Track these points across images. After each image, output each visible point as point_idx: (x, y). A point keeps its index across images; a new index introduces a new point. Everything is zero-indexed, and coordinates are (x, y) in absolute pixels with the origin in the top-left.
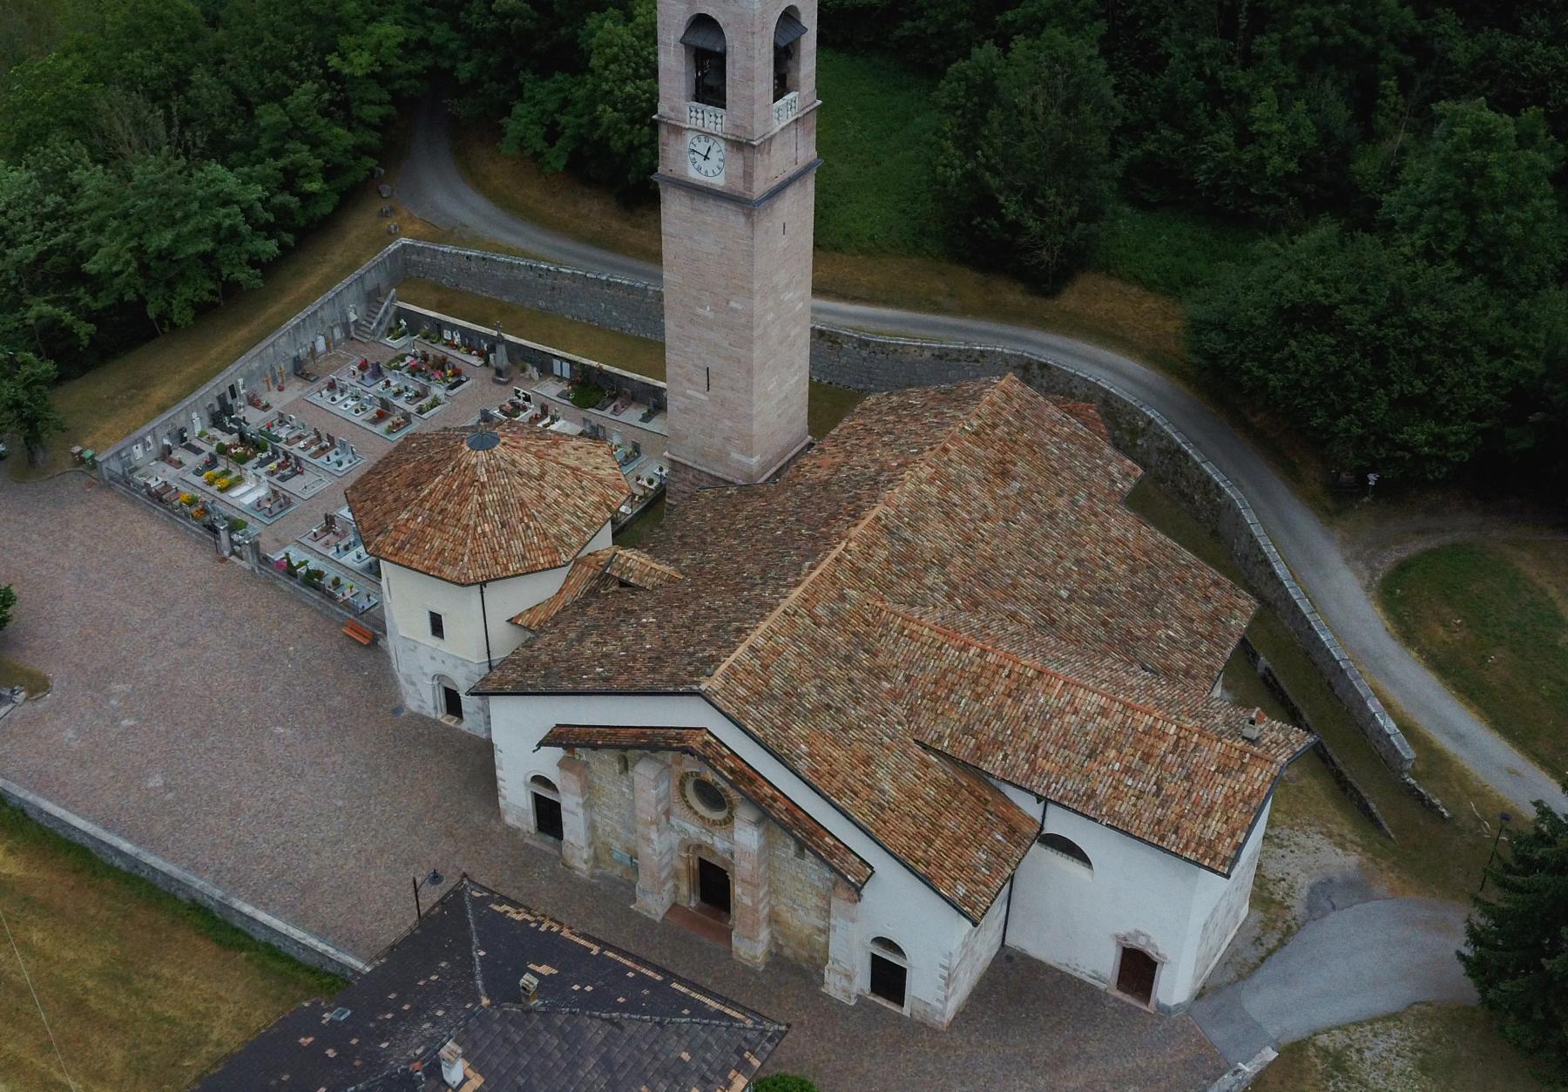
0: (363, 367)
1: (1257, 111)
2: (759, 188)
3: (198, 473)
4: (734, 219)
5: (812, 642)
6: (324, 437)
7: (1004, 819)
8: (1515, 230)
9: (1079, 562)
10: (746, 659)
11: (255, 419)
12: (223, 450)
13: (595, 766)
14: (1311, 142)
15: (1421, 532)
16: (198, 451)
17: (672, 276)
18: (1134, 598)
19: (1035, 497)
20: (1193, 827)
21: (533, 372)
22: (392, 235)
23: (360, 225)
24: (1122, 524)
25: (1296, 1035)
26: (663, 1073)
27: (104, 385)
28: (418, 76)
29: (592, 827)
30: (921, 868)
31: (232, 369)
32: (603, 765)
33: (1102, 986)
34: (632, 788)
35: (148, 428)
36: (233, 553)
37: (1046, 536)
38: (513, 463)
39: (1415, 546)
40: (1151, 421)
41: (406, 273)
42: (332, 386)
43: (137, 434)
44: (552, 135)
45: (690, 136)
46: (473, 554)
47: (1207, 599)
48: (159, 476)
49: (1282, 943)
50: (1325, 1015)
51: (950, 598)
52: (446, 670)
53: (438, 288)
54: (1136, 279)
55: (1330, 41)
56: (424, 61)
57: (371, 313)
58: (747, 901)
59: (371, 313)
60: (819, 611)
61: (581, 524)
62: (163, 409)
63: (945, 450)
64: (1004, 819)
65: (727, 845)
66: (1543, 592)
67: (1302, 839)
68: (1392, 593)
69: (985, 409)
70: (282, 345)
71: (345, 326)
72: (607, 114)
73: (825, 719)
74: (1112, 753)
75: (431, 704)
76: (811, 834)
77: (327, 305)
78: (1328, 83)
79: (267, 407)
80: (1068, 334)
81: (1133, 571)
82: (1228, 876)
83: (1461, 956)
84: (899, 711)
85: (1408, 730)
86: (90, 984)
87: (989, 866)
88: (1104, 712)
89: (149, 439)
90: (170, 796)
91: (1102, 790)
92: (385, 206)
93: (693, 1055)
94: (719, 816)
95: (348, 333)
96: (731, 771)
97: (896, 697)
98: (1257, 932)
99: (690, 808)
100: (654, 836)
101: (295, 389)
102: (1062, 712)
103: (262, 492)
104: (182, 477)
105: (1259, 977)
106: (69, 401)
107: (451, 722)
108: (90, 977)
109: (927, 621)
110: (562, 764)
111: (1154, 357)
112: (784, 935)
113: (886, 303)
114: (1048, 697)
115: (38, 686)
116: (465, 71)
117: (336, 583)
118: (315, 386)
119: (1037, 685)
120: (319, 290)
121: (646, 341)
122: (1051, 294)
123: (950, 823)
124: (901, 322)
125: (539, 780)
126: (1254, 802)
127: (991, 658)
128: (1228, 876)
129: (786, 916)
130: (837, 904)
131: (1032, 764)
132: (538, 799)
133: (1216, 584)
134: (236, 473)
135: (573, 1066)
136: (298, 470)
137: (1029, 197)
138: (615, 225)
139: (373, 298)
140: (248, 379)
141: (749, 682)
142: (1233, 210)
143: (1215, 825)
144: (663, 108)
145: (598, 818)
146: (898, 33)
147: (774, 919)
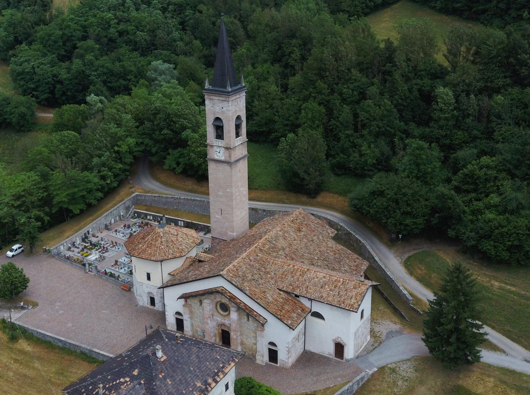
0: (125, 226)
1: (363, 148)
2: (233, 159)
3: (79, 253)
4: (227, 167)
5: (249, 265)
6: (114, 243)
7: (301, 307)
8: (430, 170)
9: (320, 251)
10: (232, 267)
11: (94, 240)
12: (85, 247)
13: (193, 305)
14: (379, 155)
15: (414, 249)
16: (78, 248)
17: (211, 198)
18: (335, 260)
19: (308, 236)
20: (348, 302)
21: (173, 224)
22: (133, 193)
23: (124, 191)
24: (332, 243)
25: (382, 365)
26: (213, 360)
27: (51, 233)
28: (141, 151)
29: (192, 325)
30: (279, 317)
31: (88, 226)
32: (194, 302)
33: (331, 357)
34: (203, 310)
35: (65, 241)
36: (89, 271)
37: (311, 245)
38: (170, 231)
39: (412, 253)
40: (341, 226)
41: (137, 202)
42: (116, 231)
43: (62, 242)
44: (178, 164)
45: (215, 148)
46: (159, 253)
47: (355, 262)
48: (69, 254)
49: (379, 345)
50: (389, 361)
51: (286, 257)
52: (150, 290)
53: (146, 205)
54: (336, 193)
55: (381, 130)
56: (142, 148)
57: (127, 213)
58: (235, 337)
59: (127, 213)
60: (251, 258)
61: (188, 247)
62: (68, 237)
63: (284, 224)
64: (301, 307)
65: (229, 322)
66: (445, 260)
67: (384, 322)
68: (407, 264)
69: (294, 216)
70: (102, 220)
71: (120, 216)
72: (193, 155)
73: (253, 283)
74: (327, 287)
75: (146, 302)
76: (250, 311)
77: (114, 211)
78: (382, 141)
79: (97, 237)
80: (320, 208)
81: (335, 254)
82: (357, 312)
83: (422, 339)
84: (273, 282)
85: (411, 294)
86: (52, 375)
87: (297, 317)
88: (324, 277)
89: (65, 244)
90: (74, 328)
91: (324, 295)
92: (131, 186)
93: (220, 357)
94: (227, 313)
95: (120, 218)
96: (229, 296)
97: (272, 278)
98: (373, 343)
99: (219, 312)
100: (209, 322)
101: (105, 233)
102: (314, 278)
103: (97, 256)
104: (75, 254)
105: (373, 353)
106: (43, 236)
107: (152, 307)
108: (52, 373)
109: (279, 261)
110: (184, 306)
111: (342, 212)
112: (245, 348)
113: (270, 202)
114: (311, 275)
115: (35, 305)
116: (154, 150)
117: (119, 276)
118: (111, 231)
119: (308, 272)
120: (112, 207)
121: (205, 215)
122: (314, 198)
123: (287, 307)
124: (274, 206)
125: (178, 313)
126: (363, 295)
127: (296, 267)
128: (357, 312)
129: (245, 341)
130: (258, 333)
131: (307, 291)
132: (177, 319)
133: (358, 258)
134: (89, 252)
135: (189, 356)
136: (107, 251)
137: (307, 172)
138: (195, 187)
139: (128, 209)
140: (93, 229)
141: (233, 273)
142: (360, 174)
143: (353, 300)
144: (208, 141)
145: (194, 322)
146: (271, 137)
147: (242, 344)
